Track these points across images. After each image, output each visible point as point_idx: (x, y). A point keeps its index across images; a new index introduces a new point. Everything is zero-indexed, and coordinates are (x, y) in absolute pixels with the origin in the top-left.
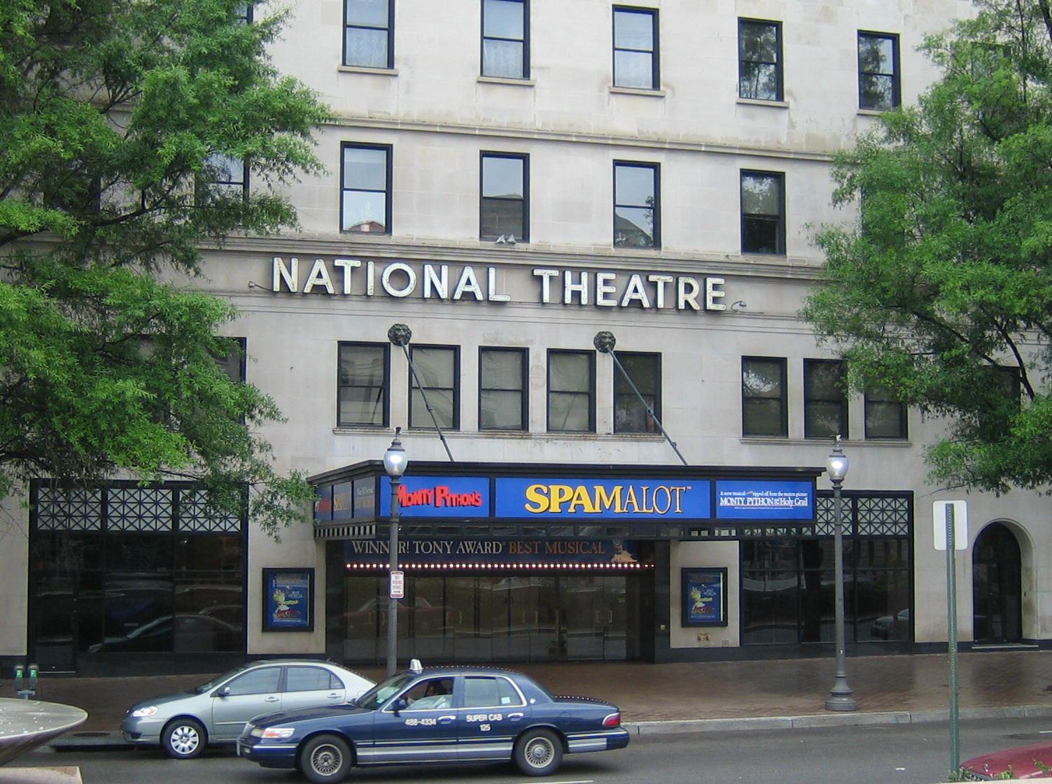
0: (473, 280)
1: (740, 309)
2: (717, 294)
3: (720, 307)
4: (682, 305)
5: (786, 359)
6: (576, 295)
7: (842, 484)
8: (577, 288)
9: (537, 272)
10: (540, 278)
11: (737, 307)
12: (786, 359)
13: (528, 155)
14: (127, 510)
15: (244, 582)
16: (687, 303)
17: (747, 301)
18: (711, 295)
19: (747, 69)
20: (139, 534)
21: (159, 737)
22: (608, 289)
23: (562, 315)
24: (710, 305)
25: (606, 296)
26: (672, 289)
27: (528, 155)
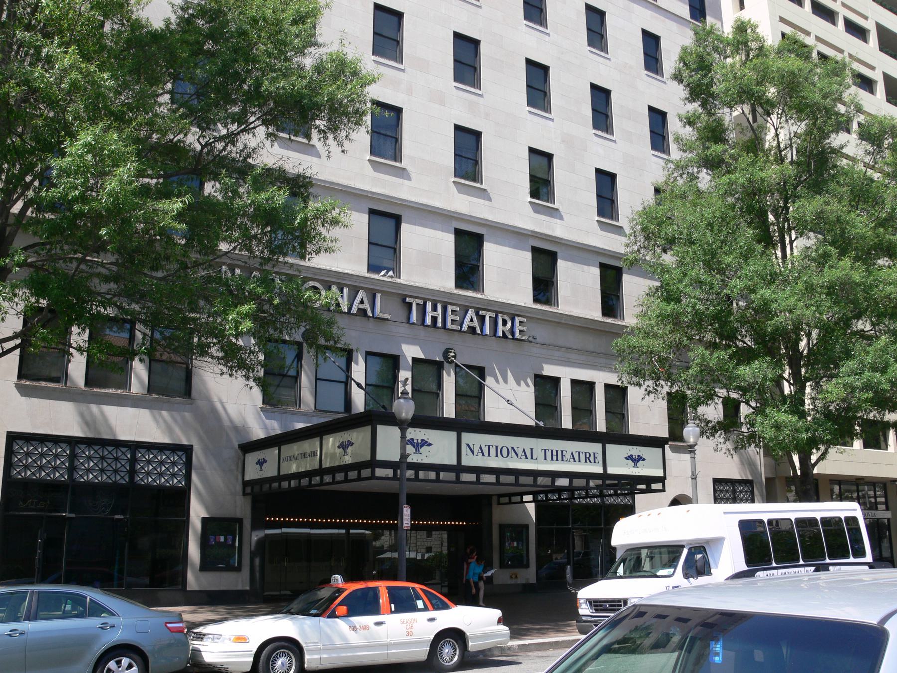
0: (365, 300)
1: (533, 340)
2: (522, 328)
3: (525, 338)
4: (500, 334)
5: (560, 378)
6: (434, 319)
7: (696, 447)
8: (434, 314)
9: (408, 300)
10: (410, 304)
11: (531, 339)
12: (560, 378)
13: (400, 216)
14: (119, 465)
15: (68, 581)
16: (503, 332)
17: (537, 336)
18: (517, 328)
19: (534, 194)
20: (161, 489)
21: (251, 659)
22: (454, 317)
23: (421, 331)
24: (517, 335)
25: (453, 321)
26: (495, 322)
27: (400, 216)
